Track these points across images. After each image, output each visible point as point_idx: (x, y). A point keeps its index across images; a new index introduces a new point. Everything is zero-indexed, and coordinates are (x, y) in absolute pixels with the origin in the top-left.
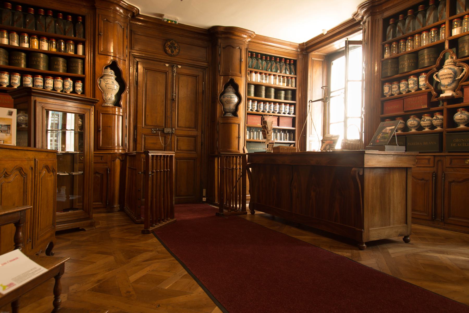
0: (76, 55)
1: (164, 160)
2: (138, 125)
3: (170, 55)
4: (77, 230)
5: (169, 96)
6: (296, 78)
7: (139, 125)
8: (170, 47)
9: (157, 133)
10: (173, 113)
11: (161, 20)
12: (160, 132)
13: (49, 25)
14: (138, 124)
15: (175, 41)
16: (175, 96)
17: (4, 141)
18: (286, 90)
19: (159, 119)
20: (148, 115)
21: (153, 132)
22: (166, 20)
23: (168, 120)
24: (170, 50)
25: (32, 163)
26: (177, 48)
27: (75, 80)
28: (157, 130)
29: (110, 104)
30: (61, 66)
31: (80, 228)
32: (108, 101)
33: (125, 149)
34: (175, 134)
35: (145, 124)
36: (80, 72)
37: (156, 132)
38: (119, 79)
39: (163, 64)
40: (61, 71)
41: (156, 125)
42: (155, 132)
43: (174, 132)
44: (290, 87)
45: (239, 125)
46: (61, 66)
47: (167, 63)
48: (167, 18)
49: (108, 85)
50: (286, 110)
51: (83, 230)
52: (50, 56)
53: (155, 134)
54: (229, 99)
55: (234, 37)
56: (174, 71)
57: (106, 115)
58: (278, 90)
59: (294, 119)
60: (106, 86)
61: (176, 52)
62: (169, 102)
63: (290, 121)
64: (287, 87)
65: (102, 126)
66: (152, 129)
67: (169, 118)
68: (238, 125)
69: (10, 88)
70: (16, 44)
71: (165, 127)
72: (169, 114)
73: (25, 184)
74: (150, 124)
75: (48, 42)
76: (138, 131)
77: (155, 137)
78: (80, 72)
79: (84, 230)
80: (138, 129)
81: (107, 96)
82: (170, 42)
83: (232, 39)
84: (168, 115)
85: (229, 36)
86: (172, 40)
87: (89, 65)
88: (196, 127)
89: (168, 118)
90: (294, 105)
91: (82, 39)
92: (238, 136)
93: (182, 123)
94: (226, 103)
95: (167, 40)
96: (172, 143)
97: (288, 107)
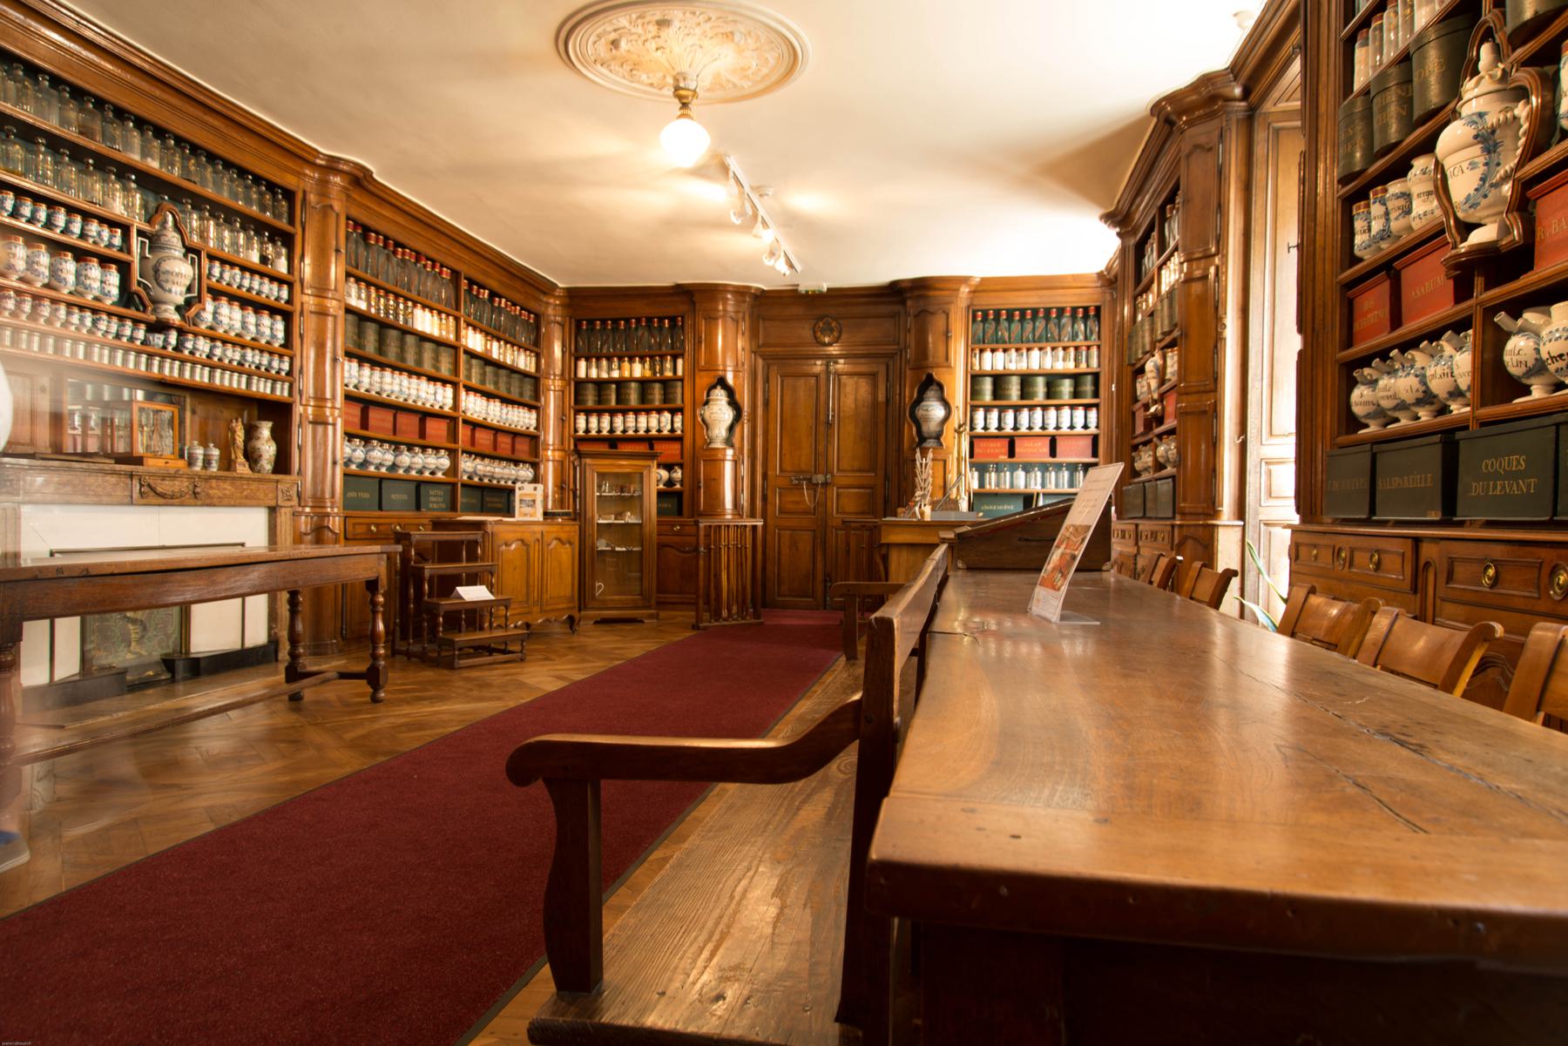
0: (675, 377)
1: (715, 532)
2: (769, 473)
5: (822, 417)
6: (1099, 347)
15: (831, 318)
17: (1271, 434)
18: (1076, 378)
19: (805, 458)
25: (539, 536)
27: (673, 412)
29: (718, 445)
30: (657, 393)
36: (679, 402)
38: (734, 403)
40: (657, 403)
43: (829, 481)
44: (1083, 367)
45: (945, 462)
46: (657, 393)
52: (644, 384)
54: (925, 413)
55: (931, 293)
58: (1053, 380)
59: (1095, 438)
62: (822, 428)
63: (1088, 442)
64: (1078, 371)
68: (942, 463)
70: (604, 375)
71: (815, 473)
72: (821, 448)
73: (528, 553)
74: (789, 468)
75: (640, 362)
78: (679, 402)
83: (928, 297)
85: (923, 292)
88: (873, 469)
90: (1096, 406)
91: (680, 352)
92: (942, 484)
93: (845, 465)
97: (1080, 413)
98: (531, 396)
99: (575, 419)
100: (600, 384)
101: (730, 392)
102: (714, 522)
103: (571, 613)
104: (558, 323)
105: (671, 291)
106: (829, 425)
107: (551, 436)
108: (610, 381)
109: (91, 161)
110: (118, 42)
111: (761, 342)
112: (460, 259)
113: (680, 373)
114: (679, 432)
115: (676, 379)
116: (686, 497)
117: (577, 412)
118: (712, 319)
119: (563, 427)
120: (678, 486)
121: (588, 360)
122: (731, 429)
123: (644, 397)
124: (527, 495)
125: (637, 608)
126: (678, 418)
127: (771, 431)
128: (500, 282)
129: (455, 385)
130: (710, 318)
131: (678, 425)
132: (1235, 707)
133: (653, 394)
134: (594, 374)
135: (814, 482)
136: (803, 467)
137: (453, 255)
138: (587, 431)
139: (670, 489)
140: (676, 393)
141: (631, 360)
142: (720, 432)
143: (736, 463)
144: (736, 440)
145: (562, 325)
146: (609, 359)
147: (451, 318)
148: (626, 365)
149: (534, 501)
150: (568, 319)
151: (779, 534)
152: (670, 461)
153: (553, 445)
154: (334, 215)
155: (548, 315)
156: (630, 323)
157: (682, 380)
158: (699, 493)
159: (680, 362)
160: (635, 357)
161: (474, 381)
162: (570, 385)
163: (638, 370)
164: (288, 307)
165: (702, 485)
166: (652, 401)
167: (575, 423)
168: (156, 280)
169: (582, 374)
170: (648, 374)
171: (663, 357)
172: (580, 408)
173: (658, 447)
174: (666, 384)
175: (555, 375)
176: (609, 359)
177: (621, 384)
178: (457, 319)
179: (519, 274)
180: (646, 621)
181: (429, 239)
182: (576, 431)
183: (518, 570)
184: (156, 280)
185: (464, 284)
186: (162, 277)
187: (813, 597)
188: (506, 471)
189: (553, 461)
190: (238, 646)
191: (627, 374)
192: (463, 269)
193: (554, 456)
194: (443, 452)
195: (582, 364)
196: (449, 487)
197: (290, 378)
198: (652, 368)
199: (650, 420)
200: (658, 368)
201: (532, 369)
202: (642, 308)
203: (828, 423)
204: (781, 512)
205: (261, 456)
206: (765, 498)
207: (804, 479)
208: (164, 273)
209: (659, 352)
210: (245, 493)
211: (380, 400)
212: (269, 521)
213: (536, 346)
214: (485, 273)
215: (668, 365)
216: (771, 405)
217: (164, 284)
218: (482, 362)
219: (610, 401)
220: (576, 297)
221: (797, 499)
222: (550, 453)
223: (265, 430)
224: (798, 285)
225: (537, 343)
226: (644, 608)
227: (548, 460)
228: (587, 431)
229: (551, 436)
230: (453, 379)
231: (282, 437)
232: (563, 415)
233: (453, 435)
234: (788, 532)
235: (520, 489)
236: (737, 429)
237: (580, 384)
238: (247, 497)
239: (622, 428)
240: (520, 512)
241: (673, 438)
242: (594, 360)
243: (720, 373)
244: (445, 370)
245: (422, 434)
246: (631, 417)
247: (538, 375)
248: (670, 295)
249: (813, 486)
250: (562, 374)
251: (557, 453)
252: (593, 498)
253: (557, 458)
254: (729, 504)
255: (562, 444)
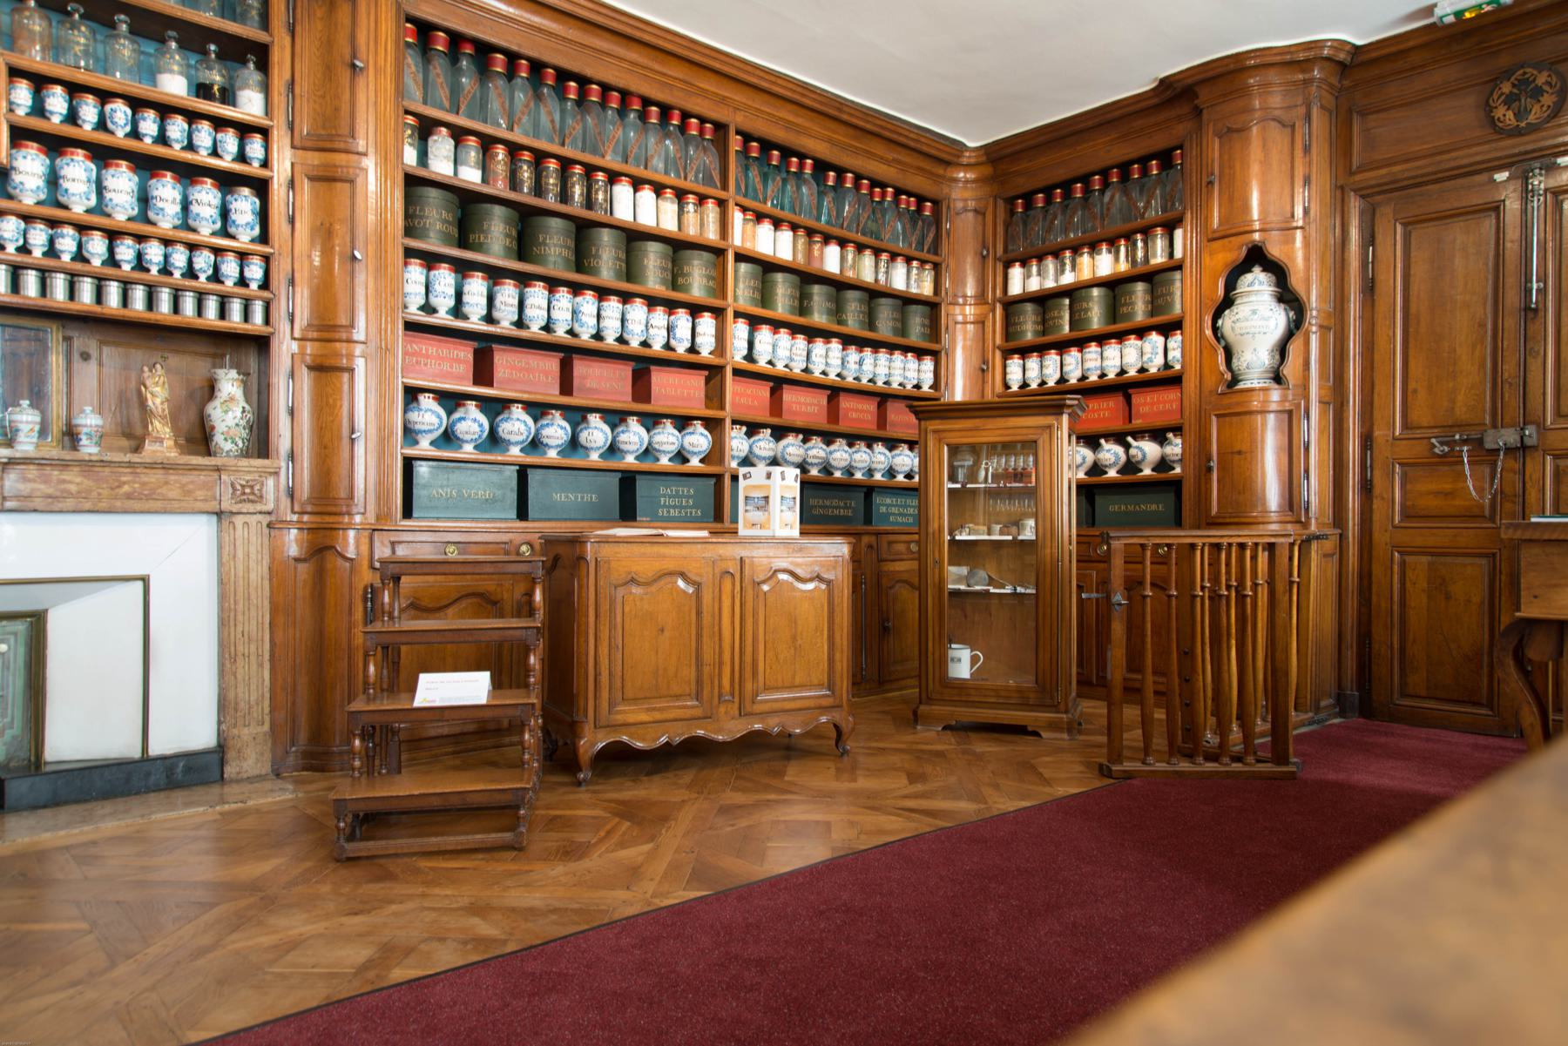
2: (1377, 433)
3: (1517, 132)
4: (1019, 730)
5: (1512, 298)
7: (1381, 433)
8: (1509, 101)
9: (1456, 454)
10: (1535, 365)
11: (1433, 25)
12: (1465, 448)
13: (1108, 209)
14: (1375, 428)
16: (1542, 292)
20: (1415, 391)
21: (1437, 450)
22: (1451, 19)
23: (1507, 395)
24: (1510, 114)
26: (1546, 88)
28: (1455, 441)
31: (1030, 729)
32: (1246, 374)
33: (1303, 520)
34: (1544, 451)
35: (1406, 425)
37: (1452, 450)
38: (1287, 296)
39: (1483, 178)
41: (1450, 423)
42: (1446, 449)
43: (1528, 442)
47: (1500, 168)
48: (1449, 10)
49: (1238, 325)
50: (923, 376)
51: (1036, 734)
52: (1114, 286)
53: (1445, 455)
56: (1532, 191)
57: (1227, 419)
60: (1233, 329)
61: (1545, 109)
62: (1511, 323)
65: (1218, 454)
66: (1433, 441)
67: (1510, 384)
69: (1142, 375)
72: (1509, 369)
76: (1376, 452)
77: (1446, 468)
78: (1177, 309)
79: (1039, 735)
80: (1374, 445)
81: (1242, 359)
82: (1509, 80)
84: (1506, 375)
86: (1522, 67)
87: (1191, 281)
89: (1506, 386)
94: (1239, 337)
95: (1496, 79)
96: (1528, 486)
98: (508, 250)
99: (1005, 367)
100: (1043, 300)
101: (1278, 272)
102: (1246, 535)
103: (837, 716)
105: (1155, 101)
106: (1530, 312)
109: (213, 47)
110: (631, 22)
111: (1356, 162)
112: (723, 100)
113: (1178, 254)
114: (1178, 367)
116: (1188, 490)
118: (1234, 133)
119: (984, 382)
120: (1178, 470)
121: (1024, 264)
122: (1282, 350)
123: (1114, 310)
124: (755, 487)
125: (1025, 705)
127: (1381, 340)
128: (830, 141)
129: (718, 313)
130: (1230, 130)
131: (1175, 354)
133: (1133, 304)
135: (1489, 445)
136: (1461, 412)
137: (704, 94)
139: (1163, 476)
140: (1171, 294)
142: (1255, 356)
143: (1290, 418)
144: (1290, 370)
147: (710, 205)
149: (766, 498)
151: (1403, 564)
152: (1159, 422)
157: (1179, 267)
158: (1209, 481)
161: (780, 310)
162: (994, 311)
163: (1105, 264)
164: (264, 173)
165: (1214, 464)
166: (1129, 316)
167: (1005, 373)
169: (1015, 289)
170: (1123, 266)
173: (1142, 400)
174: (1153, 277)
175: (965, 296)
177: (1073, 293)
178: (721, 203)
179: (869, 127)
180: (1043, 734)
181: (632, 63)
183: (667, 634)
185: (735, 143)
187: (1490, 706)
190: (136, 753)
192: (735, 119)
196: (712, 481)
197: (266, 294)
199: (1125, 351)
201: (927, 289)
203: (1527, 309)
204: (1407, 515)
205: (213, 428)
206: (1366, 487)
207: (1464, 442)
210: (126, 488)
211: (889, 392)
213: (930, 254)
214: (789, 126)
216: (1381, 288)
218: (758, 269)
219: (1060, 327)
220: (1000, 156)
221: (1447, 487)
224: (1429, 10)
226: (1041, 706)
230: (717, 303)
232: (985, 362)
233: (715, 395)
234: (1425, 559)
235: (745, 477)
236: (1294, 348)
237: (1011, 306)
238: (129, 496)
239: (1057, 376)
240: (745, 519)
241: (1169, 379)
243: (1257, 236)
244: (697, 288)
245: (566, 386)
247: (937, 300)
249: (1485, 455)
252: (941, 495)
254: (1273, 495)
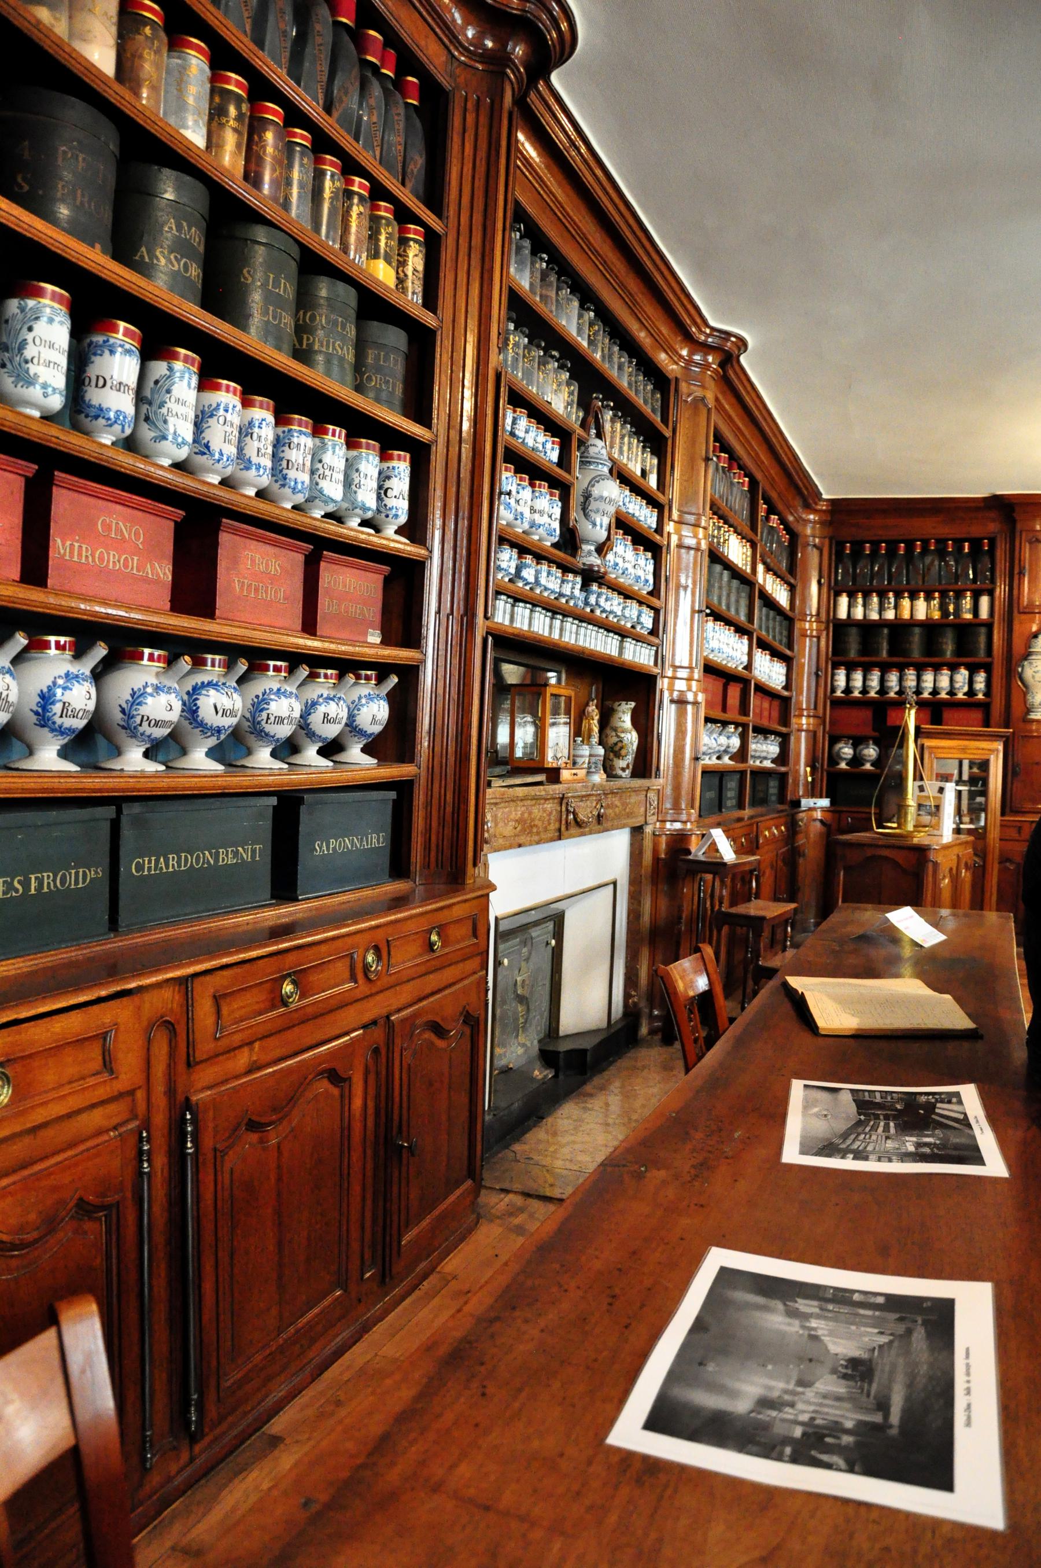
52: (929, 628)
70: (874, 616)
100: (867, 628)
104: (815, 546)
107: (804, 698)
108: (882, 623)
115: (976, 624)
117: (836, 666)
126: (980, 679)
132: (858, 908)
134: (859, 613)
138: (848, 690)
141: (913, 597)
145: (820, 549)
146: (882, 595)
148: (906, 603)
150: (827, 541)
153: (808, 709)
154: (705, 412)
155: (806, 536)
156: (914, 547)
159: (984, 601)
160: (903, 592)
168: (584, 509)
171: (959, 595)
172: (838, 657)
176: (882, 595)
182: (833, 690)
184: (584, 509)
186: (593, 505)
188: (764, 747)
189: (807, 731)
191: (906, 615)
193: (808, 724)
194: (731, 728)
195: (844, 601)
198: (943, 608)
200: (951, 608)
202: (932, 527)
208: (596, 500)
209: (956, 587)
212: (632, 845)
215: (967, 602)
217: (592, 514)
222: (804, 720)
223: (624, 716)
225: (792, 569)
227: (800, 730)
228: (848, 690)
229: (804, 698)
231: (644, 722)
232: (818, 669)
239: (897, 689)
242: (860, 595)
246: (946, 673)
248: (977, 509)
250: (818, 614)
251: (811, 720)
253: (811, 728)
255: (815, 708)
